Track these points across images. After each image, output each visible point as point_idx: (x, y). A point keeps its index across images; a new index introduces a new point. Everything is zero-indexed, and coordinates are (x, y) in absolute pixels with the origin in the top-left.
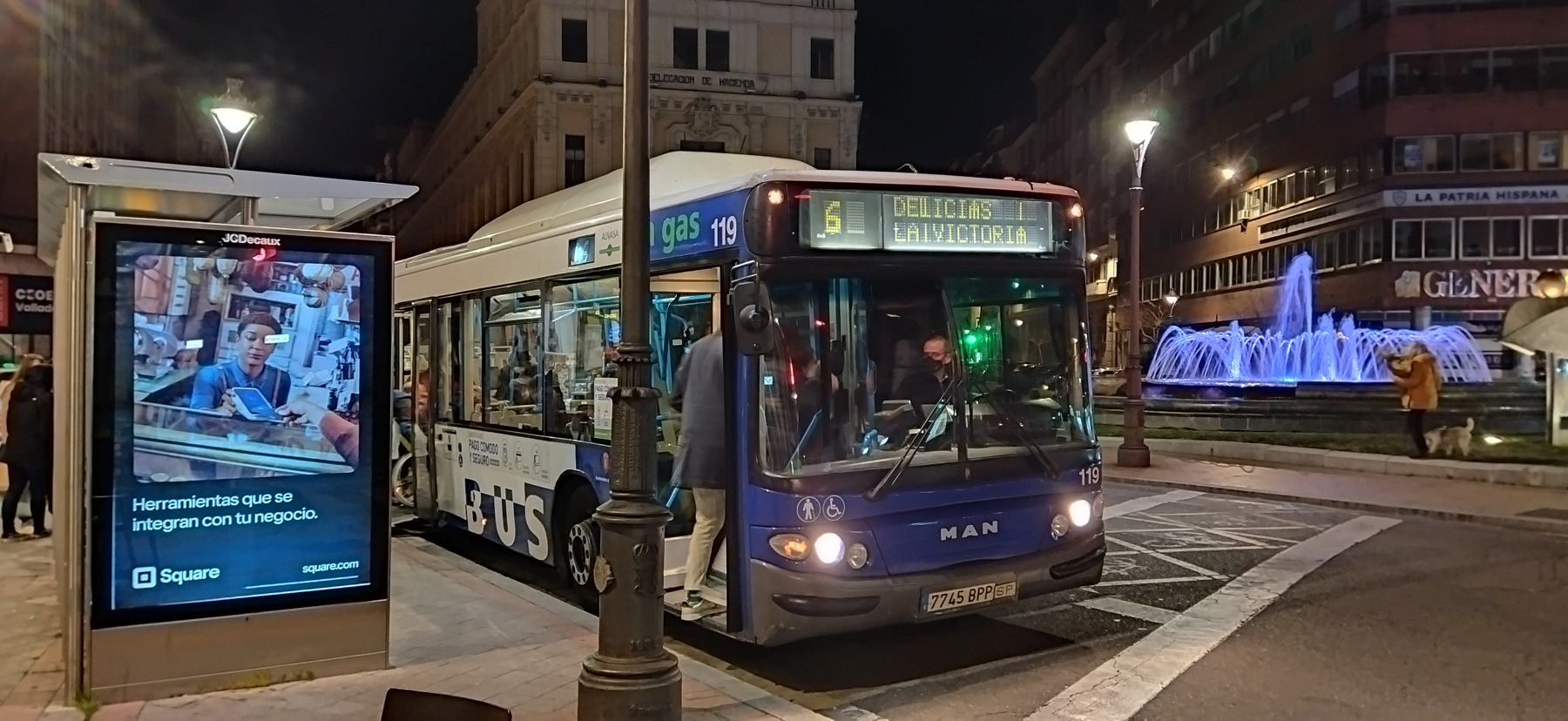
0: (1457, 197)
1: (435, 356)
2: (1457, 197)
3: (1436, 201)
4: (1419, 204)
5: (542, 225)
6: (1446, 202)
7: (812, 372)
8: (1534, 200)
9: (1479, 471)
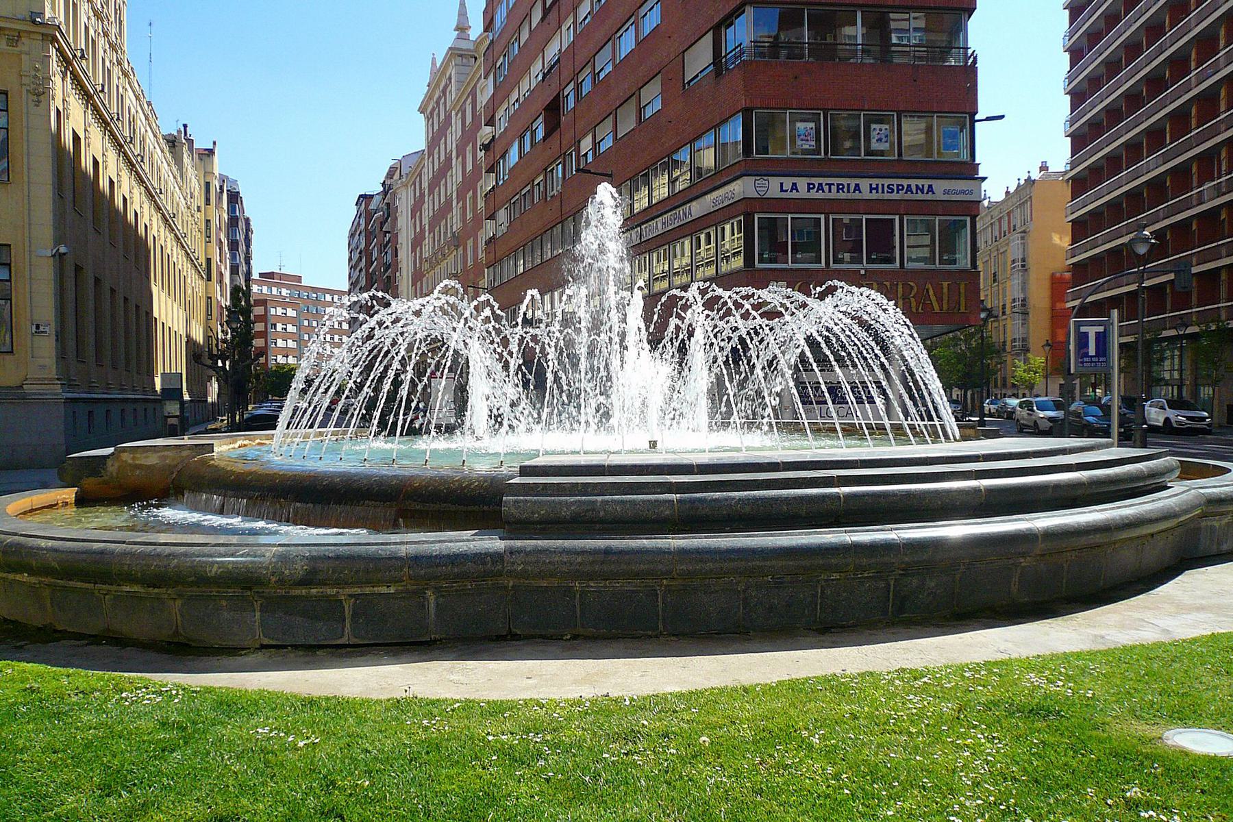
0: (826, 188)
1: (797, 47)
2: (826, 188)
3: (803, 193)
4: (784, 195)
5: (341, 459)
6: (814, 194)
7: (573, 327)
8: (909, 196)
9: (497, 710)
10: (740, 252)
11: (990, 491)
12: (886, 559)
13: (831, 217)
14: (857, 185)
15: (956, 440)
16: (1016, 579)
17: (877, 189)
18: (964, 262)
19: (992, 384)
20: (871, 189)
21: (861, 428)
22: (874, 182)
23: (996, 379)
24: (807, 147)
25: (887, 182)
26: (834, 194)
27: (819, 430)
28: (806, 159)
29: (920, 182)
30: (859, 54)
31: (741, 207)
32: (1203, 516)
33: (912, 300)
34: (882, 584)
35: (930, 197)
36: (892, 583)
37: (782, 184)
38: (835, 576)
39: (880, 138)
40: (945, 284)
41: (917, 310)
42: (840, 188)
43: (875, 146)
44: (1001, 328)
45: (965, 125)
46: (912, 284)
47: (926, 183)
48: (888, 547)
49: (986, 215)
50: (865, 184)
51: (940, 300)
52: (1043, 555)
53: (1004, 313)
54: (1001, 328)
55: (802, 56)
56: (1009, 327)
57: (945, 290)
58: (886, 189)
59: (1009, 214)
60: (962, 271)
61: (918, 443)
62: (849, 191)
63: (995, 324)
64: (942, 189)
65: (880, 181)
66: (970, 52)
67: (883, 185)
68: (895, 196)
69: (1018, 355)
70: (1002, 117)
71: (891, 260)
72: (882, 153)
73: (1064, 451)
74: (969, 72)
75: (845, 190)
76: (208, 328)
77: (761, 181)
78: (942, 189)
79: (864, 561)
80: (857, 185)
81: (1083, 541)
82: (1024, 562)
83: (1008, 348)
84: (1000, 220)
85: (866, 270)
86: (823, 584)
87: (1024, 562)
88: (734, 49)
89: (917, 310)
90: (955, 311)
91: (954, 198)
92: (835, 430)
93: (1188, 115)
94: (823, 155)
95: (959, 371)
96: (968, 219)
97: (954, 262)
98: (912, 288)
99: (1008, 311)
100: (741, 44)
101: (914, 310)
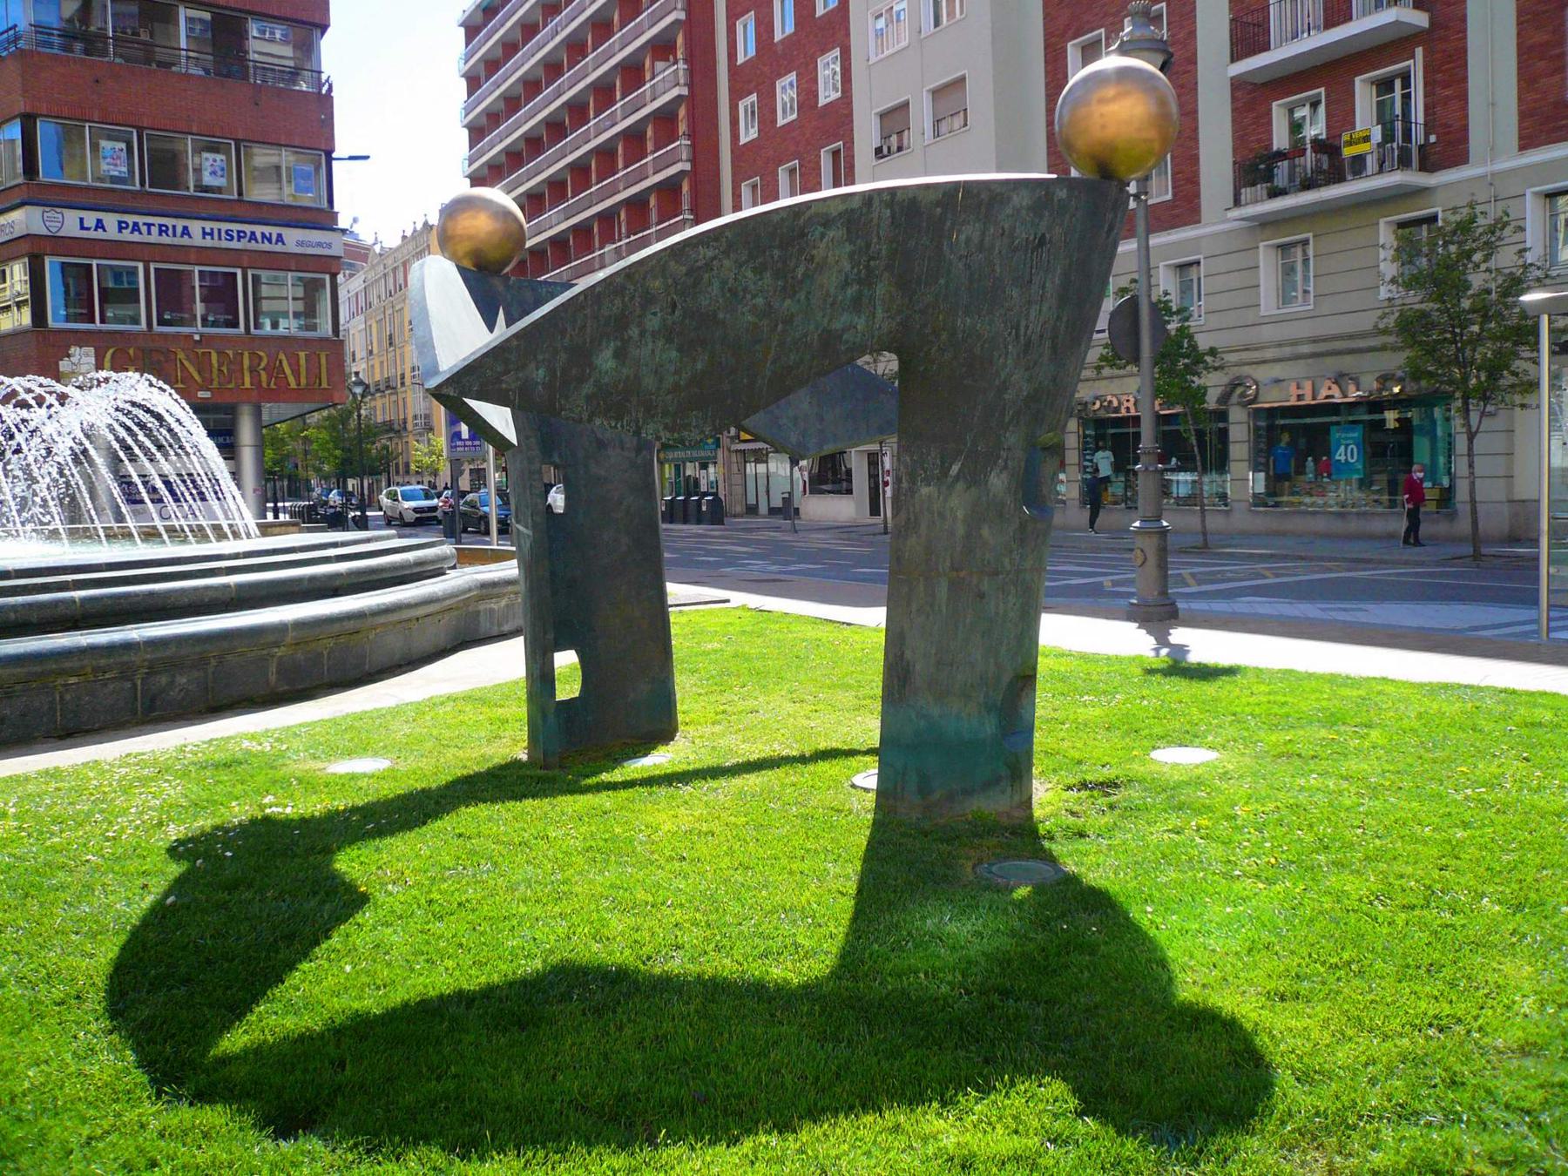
0: (144, 229)
2: (144, 229)
3: (112, 233)
4: (85, 234)
6: (127, 236)
8: (253, 246)
10: (26, 301)
11: (240, 586)
12: (125, 658)
13: (152, 266)
14: (185, 228)
15: (248, 536)
16: (273, 668)
17: (211, 234)
18: (325, 329)
19: (393, 469)
20: (205, 234)
21: (183, 530)
22: (208, 225)
23: (397, 464)
24: (116, 173)
25: (225, 226)
26: (154, 237)
27: (115, 536)
28: (113, 190)
29: (267, 230)
30: (183, 61)
31: (25, 247)
32: (481, 598)
33: (263, 373)
34: (128, 685)
35: (279, 248)
36: (139, 682)
37: (82, 220)
38: (73, 680)
39: (209, 169)
40: (302, 355)
41: (269, 384)
42: (163, 230)
43: (208, 179)
44: (401, 403)
45: (320, 164)
46: (261, 354)
47: (274, 231)
48: (128, 646)
49: (378, 263)
50: (196, 227)
51: (296, 374)
52: (297, 644)
53: (403, 384)
54: (401, 403)
55: (105, 53)
56: (409, 400)
57: (303, 362)
58: (223, 234)
59: (405, 264)
60: (322, 340)
61: (198, 542)
62: (174, 235)
63: (394, 398)
64: (294, 240)
65: (216, 225)
66: (324, 77)
67: (219, 230)
68: (235, 245)
69: (421, 434)
70: (367, 158)
71: (235, 325)
72: (219, 190)
73: (335, 545)
74: (324, 102)
75: (170, 232)
76: (1047, 818)
77: (52, 213)
78: (294, 240)
79: (103, 662)
80: (185, 228)
81: (337, 627)
82: (279, 652)
83: (410, 427)
84: (395, 269)
85: (202, 335)
86: (61, 689)
87: (279, 652)
88: (6, 31)
89: (269, 384)
90: (316, 386)
91: (310, 251)
92: (130, 535)
93: (587, 170)
94: (138, 186)
95: (336, 457)
96: (327, 277)
97: (314, 328)
98: (260, 358)
99: (408, 381)
100: (15, 26)
101: (264, 385)
